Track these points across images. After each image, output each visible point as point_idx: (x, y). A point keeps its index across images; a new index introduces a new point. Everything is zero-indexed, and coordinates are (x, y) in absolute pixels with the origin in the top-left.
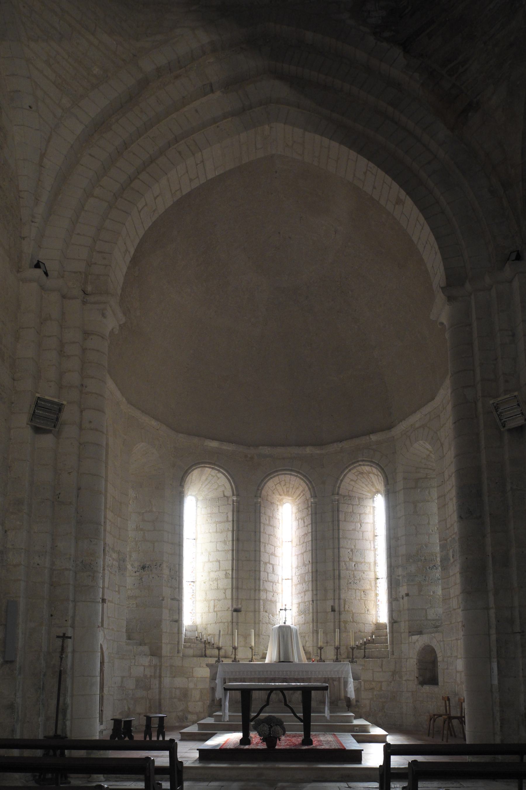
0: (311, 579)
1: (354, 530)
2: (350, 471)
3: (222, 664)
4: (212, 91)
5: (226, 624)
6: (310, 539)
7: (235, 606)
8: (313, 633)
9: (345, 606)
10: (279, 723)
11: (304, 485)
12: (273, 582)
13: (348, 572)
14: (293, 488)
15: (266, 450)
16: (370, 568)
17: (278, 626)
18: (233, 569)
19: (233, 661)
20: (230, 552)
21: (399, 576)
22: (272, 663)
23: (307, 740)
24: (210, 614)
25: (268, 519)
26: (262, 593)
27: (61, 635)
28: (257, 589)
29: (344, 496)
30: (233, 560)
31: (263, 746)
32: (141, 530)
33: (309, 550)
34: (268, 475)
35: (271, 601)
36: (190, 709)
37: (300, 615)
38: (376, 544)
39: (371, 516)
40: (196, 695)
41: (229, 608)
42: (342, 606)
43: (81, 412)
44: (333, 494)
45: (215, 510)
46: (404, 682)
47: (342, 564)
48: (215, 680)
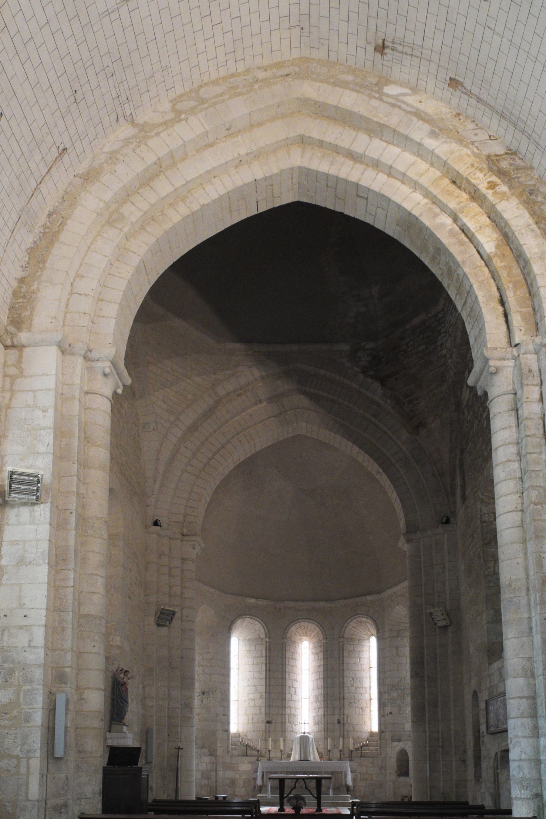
0: (323, 700)
1: (355, 663)
2: (352, 620)
3: (261, 762)
4: (261, 402)
5: (261, 732)
6: (322, 670)
7: (267, 719)
8: (324, 739)
9: (347, 720)
10: (303, 799)
11: (318, 630)
12: (295, 701)
13: (350, 694)
14: (310, 631)
15: (291, 604)
16: (366, 692)
17: (299, 735)
18: (266, 692)
19: (268, 760)
20: (264, 679)
21: (385, 699)
22: (296, 761)
23: (319, 809)
24: (249, 725)
25: (291, 654)
26: (287, 709)
27: (178, 747)
28: (284, 707)
29: (348, 639)
30: (266, 685)
31: (292, 812)
32: (202, 666)
33: (322, 678)
34: (293, 622)
35: (294, 715)
36: (237, 794)
37: (315, 725)
38: (371, 673)
39: (367, 653)
40: (241, 783)
41: (263, 721)
42: (345, 719)
43: (182, 610)
44: (339, 637)
45: (253, 648)
46: (388, 774)
47: (346, 689)
48: (257, 772)
